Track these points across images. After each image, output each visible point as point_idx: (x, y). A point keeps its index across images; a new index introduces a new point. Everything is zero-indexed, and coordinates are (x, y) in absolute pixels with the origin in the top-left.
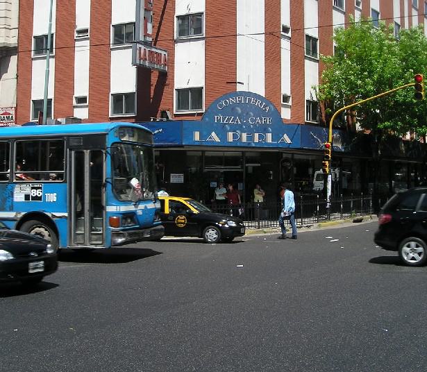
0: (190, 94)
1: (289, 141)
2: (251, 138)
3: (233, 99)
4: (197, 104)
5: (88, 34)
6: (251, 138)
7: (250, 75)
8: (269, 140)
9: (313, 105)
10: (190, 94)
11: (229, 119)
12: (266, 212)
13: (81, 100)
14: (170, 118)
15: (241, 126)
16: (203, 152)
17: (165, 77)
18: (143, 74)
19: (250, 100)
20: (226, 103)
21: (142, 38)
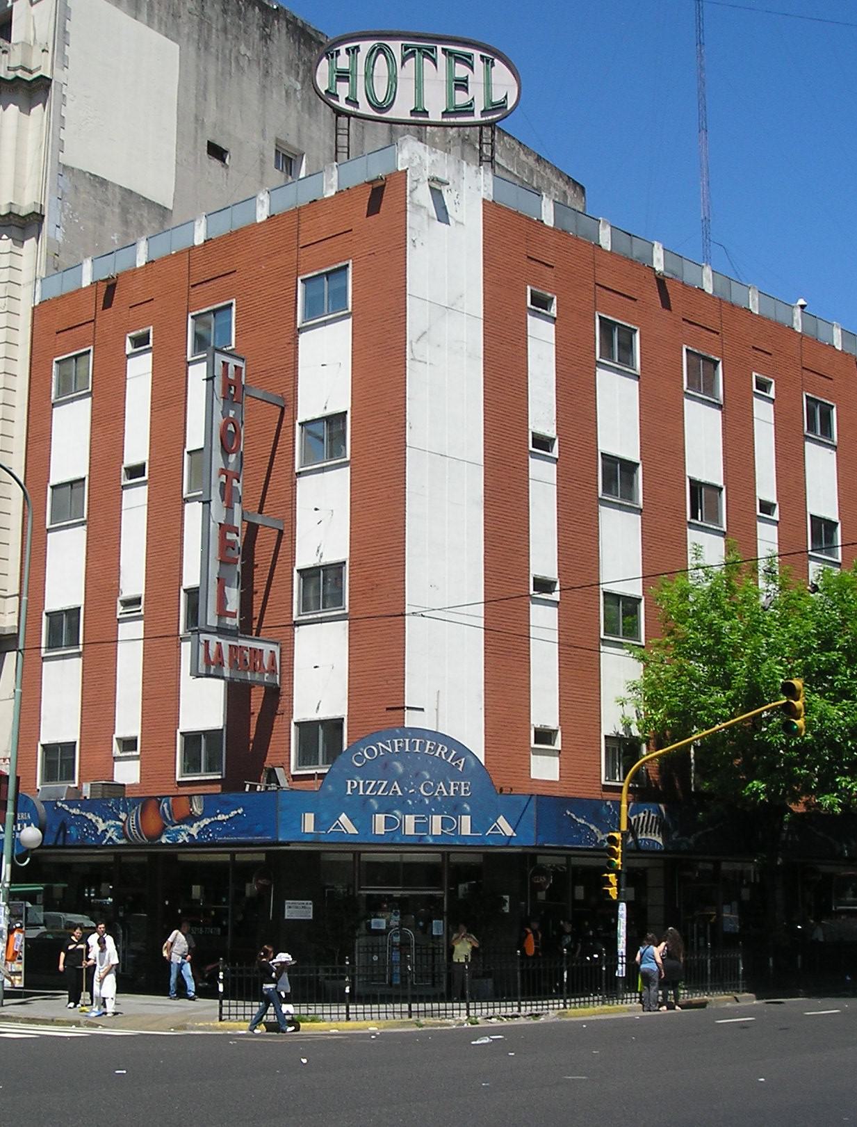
0: (321, 732)
1: (509, 831)
2: (422, 826)
3: (387, 744)
4: (334, 750)
5: (141, 607)
6: (422, 826)
7: (446, 690)
8: (466, 830)
9: (623, 749)
10: (321, 732)
11: (376, 788)
12: (489, 984)
13: (129, 744)
14: (284, 783)
15: (405, 802)
16: (357, 854)
17: (277, 697)
18: (237, 697)
19: (423, 746)
20: (370, 752)
21: (213, 621)
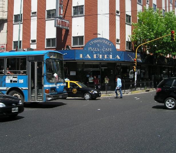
0: (78, 39)
1: (119, 58)
2: (103, 57)
3: (96, 41)
4: (81, 43)
5: (36, 14)
6: (103, 57)
7: (103, 31)
8: (111, 58)
9: (129, 43)
10: (78, 39)
11: (94, 49)
12: (110, 87)
13: (34, 41)
14: (70, 49)
15: (100, 52)
16: (84, 62)
17: (68, 32)
18: (59, 31)
19: (103, 41)
20: (93, 42)
21: (58, 16)
